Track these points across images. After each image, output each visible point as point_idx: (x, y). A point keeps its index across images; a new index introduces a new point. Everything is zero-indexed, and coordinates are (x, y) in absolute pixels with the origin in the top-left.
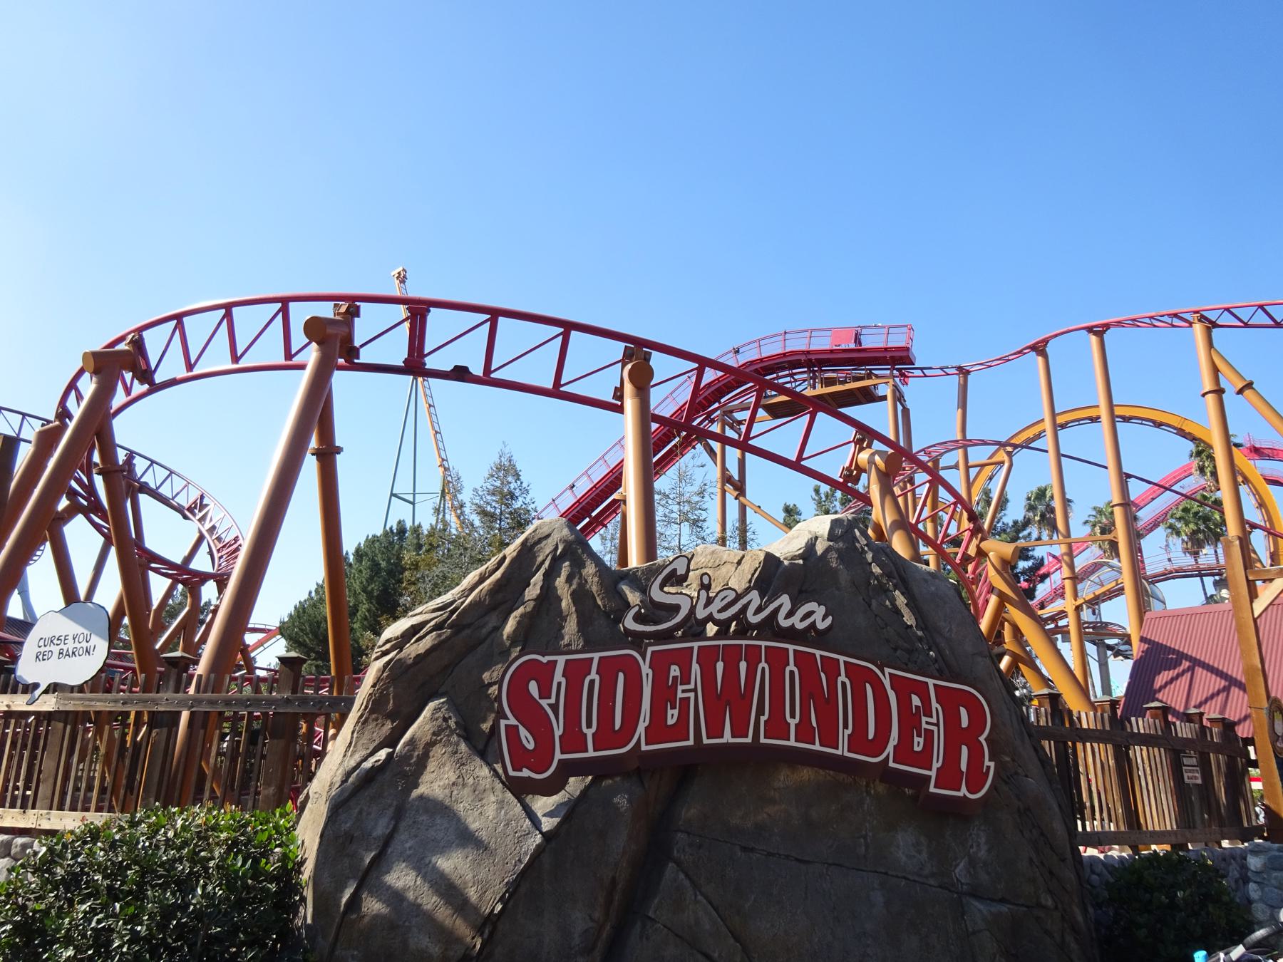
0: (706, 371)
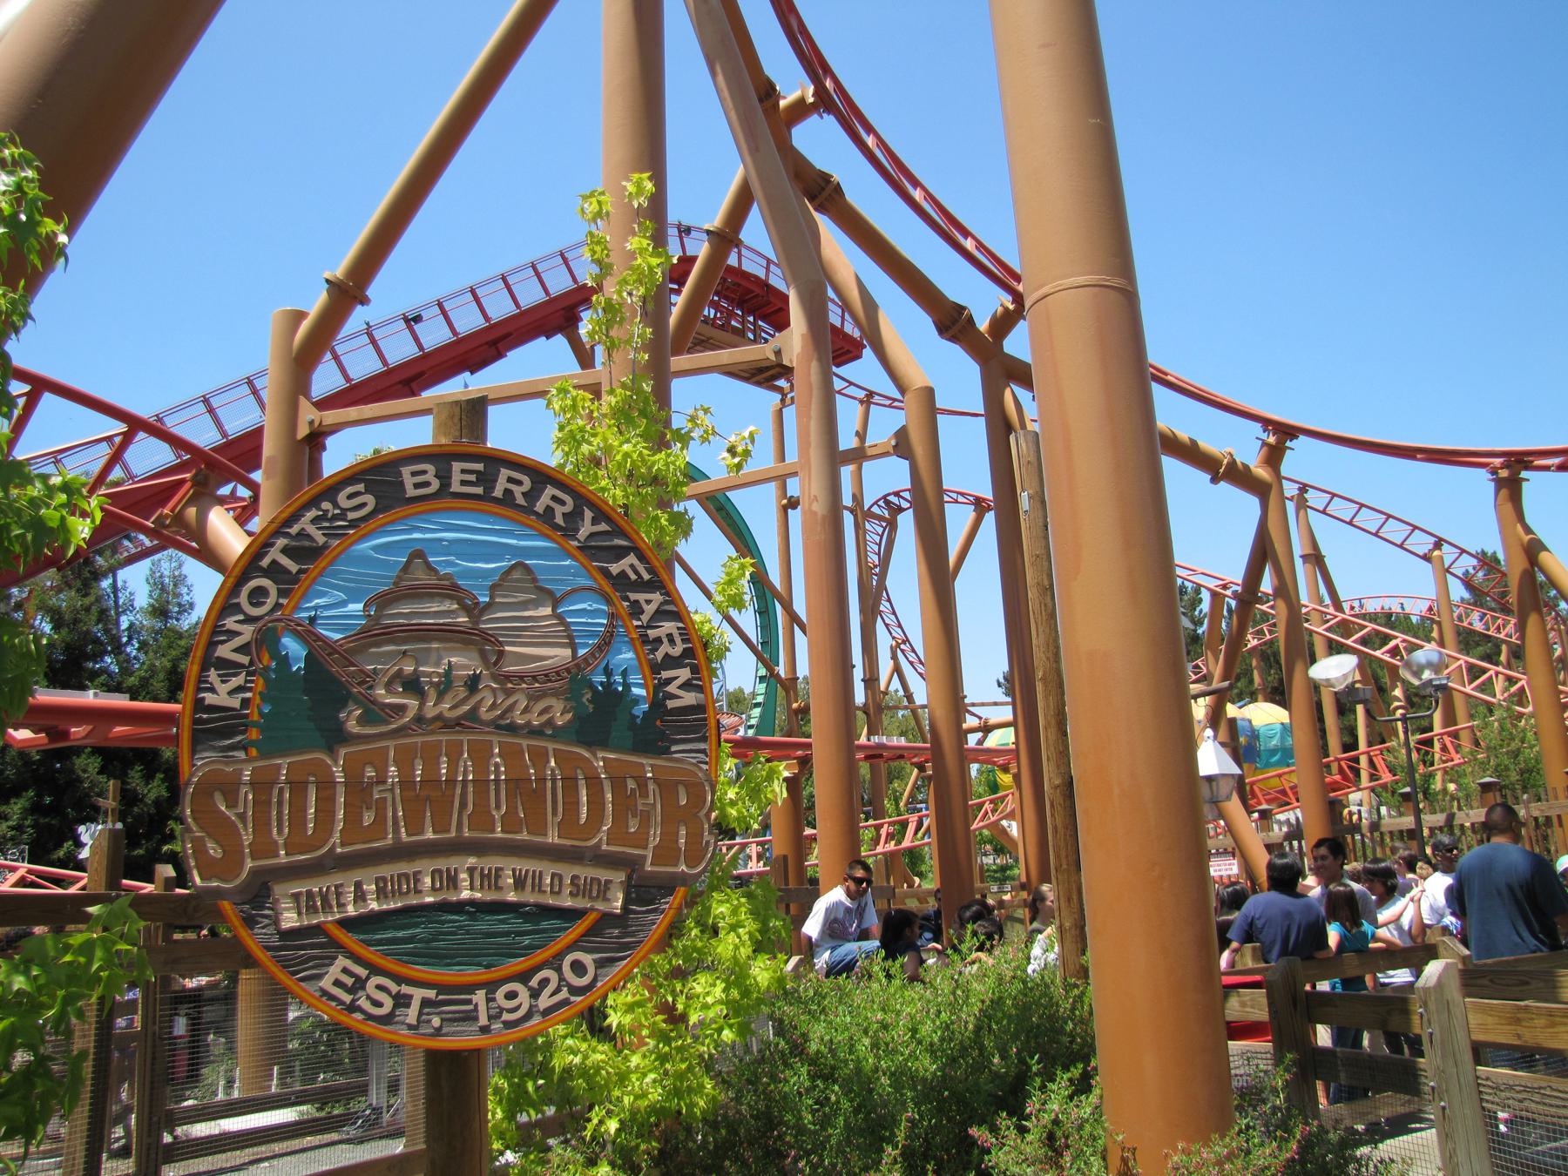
0: (137, 438)
